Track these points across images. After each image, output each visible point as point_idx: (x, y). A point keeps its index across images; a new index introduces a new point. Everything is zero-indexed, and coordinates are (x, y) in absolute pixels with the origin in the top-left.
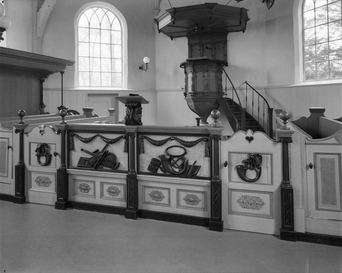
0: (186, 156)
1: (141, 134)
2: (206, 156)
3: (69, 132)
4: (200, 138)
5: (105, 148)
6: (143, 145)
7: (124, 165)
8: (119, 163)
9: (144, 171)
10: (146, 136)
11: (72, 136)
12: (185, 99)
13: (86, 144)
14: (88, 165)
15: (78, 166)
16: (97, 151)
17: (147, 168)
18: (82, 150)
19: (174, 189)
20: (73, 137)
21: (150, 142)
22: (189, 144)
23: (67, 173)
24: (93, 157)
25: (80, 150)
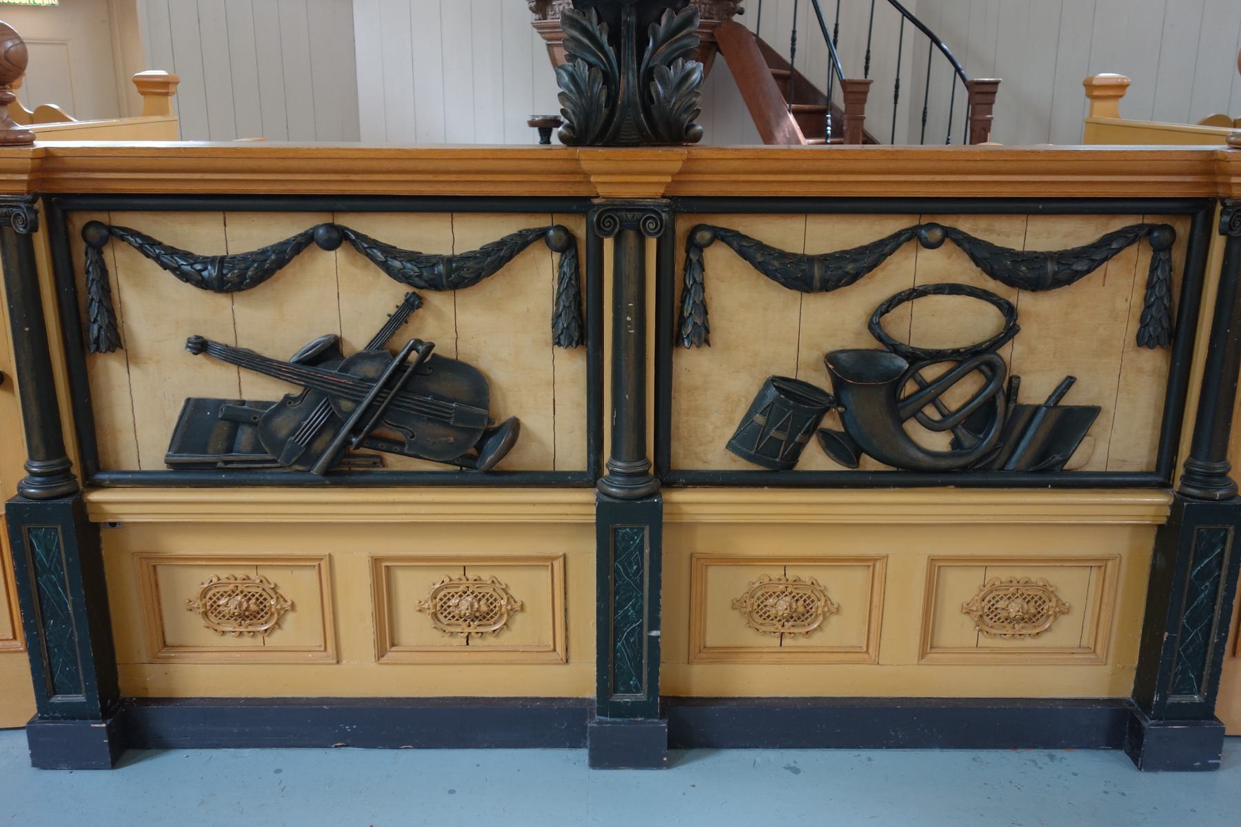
0: (1005, 352)
2: (1144, 340)
4: (1117, 224)
5: (399, 319)
7: (547, 436)
8: (515, 425)
9: (700, 466)
10: (723, 222)
11: (96, 248)
12: (538, 27)
13: (222, 300)
14: (257, 448)
15: (176, 466)
16: (330, 351)
18: (200, 346)
19: (918, 551)
20: (100, 253)
22: (1051, 267)
23: (92, 519)
24: (296, 391)
25: (177, 345)
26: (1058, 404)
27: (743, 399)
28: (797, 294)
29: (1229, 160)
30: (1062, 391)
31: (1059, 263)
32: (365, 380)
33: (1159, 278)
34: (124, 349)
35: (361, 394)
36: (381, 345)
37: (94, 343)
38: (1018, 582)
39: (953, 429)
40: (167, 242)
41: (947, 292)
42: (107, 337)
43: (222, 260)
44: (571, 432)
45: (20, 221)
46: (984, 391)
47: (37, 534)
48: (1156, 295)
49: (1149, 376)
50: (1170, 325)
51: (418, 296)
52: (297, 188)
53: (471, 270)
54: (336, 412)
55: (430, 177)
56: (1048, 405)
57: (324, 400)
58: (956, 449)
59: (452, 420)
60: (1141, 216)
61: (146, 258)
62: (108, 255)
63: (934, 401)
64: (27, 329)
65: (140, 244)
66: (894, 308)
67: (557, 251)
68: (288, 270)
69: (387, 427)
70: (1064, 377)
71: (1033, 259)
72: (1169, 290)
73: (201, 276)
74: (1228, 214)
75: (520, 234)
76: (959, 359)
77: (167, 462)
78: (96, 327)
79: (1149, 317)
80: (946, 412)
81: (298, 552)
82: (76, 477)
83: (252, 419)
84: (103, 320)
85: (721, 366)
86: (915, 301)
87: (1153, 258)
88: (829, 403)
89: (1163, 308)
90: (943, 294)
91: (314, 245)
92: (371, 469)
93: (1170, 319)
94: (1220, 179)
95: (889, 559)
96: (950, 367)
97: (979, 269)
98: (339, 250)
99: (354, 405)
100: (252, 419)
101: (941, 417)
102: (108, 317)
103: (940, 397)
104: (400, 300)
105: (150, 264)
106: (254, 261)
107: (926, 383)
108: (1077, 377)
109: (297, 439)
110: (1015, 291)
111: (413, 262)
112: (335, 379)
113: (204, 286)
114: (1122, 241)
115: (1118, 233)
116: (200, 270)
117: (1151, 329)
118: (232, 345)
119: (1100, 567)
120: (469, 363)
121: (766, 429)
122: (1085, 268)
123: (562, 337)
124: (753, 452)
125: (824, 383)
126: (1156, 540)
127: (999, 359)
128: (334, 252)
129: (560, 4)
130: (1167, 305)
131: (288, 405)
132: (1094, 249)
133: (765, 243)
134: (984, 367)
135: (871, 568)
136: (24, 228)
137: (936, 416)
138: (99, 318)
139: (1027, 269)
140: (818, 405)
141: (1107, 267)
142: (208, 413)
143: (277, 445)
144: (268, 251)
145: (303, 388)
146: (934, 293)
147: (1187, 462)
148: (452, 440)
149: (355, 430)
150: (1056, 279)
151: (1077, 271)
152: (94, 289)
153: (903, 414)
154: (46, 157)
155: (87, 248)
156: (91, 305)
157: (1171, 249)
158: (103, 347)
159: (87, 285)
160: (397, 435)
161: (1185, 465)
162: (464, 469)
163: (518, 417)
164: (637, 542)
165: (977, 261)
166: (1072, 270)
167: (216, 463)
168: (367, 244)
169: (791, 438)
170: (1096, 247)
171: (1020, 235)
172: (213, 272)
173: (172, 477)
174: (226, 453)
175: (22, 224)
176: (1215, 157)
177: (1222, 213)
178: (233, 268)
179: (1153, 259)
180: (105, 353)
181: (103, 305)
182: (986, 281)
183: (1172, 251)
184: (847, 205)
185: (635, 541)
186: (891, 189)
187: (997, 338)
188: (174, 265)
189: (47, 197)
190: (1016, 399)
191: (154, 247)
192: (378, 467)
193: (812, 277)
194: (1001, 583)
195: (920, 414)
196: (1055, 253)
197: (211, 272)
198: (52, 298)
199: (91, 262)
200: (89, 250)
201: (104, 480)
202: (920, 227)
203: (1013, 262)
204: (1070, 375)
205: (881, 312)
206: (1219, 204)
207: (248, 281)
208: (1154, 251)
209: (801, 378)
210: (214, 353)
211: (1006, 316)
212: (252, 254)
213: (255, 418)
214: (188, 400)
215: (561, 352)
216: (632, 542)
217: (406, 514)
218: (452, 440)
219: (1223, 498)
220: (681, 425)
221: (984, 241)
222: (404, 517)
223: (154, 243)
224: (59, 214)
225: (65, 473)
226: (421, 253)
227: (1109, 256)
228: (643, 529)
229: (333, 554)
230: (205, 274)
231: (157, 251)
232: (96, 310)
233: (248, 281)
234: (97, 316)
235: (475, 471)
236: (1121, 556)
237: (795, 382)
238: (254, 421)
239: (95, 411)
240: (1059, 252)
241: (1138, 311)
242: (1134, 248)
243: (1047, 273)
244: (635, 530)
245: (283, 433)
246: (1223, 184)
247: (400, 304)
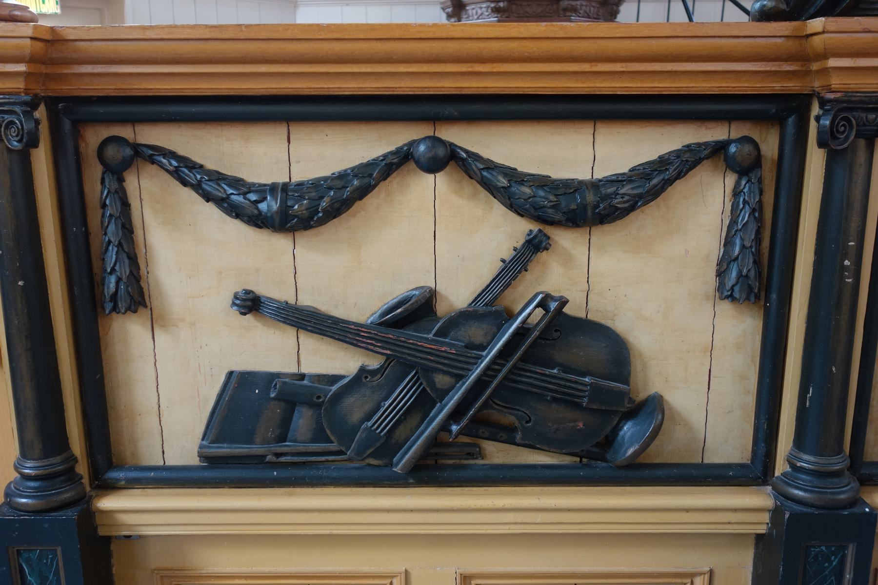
3: (78, 124)
7: (696, 418)
13: (280, 242)
14: (319, 435)
15: (211, 461)
20: (121, 180)
23: (102, 532)
24: (374, 362)
32: (471, 346)
34: (149, 308)
35: (466, 366)
36: (490, 300)
37: (111, 301)
40: (210, 165)
42: (129, 293)
43: (285, 187)
44: (729, 412)
45: (13, 131)
47: (29, 557)
51: (545, 235)
52: (397, 86)
53: (627, 198)
54: (428, 389)
55: (586, 67)
57: (413, 374)
59: (586, 400)
61: (181, 186)
62: (131, 182)
64: (21, 283)
65: (175, 167)
67: (734, 170)
68: (371, 201)
69: (495, 409)
73: (257, 208)
75: (688, 148)
77: (201, 456)
78: (113, 279)
81: (366, 569)
82: (82, 478)
83: (315, 399)
84: (124, 270)
91: (412, 165)
92: (466, 462)
98: (440, 176)
99: (453, 380)
100: (315, 399)
102: (130, 266)
104: (520, 242)
105: (188, 194)
106: (330, 188)
109: (376, 426)
111: (545, 188)
112: (433, 347)
113: (259, 223)
116: (255, 201)
118: (292, 301)
120: (603, 322)
123: (737, 289)
128: (432, 176)
129: (473, 9)
131: (364, 380)
136: (20, 141)
138: (117, 268)
142: (257, 391)
143: (347, 434)
144: (349, 174)
145: (385, 358)
148: (581, 425)
149: (456, 415)
152: (112, 228)
154: (54, 41)
155: (104, 173)
156: (107, 250)
158: (122, 305)
159: (102, 223)
160: (510, 419)
162: (584, 460)
163: (662, 393)
164: (834, 563)
167: (265, 456)
168: (483, 164)
172: (273, 203)
173: (207, 474)
174: (278, 442)
175: (17, 136)
178: (302, 197)
180: (124, 314)
181: (123, 250)
185: (830, 562)
188: (220, 194)
189: (52, 102)
191: (194, 171)
192: (476, 458)
197: (269, 206)
198: (55, 241)
199: (109, 192)
200: (106, 176)
201: (118, 480)
207: (321, 215)
210: (267, 312)
212: (325, 179)
213: (319, 397)
214: (231, 374)
215: (726, 307)
216: (827, 564)
217: (516, 523)
218: (581, 425)
222: (513, 527)
223: (193, 166)
224: (67, 125)
225: (69, 474)
226: (550, 177)
228: (845, 548)
229: (410, 571)
230: (263, 206)
231: (199, 177)
232: (114, 256)
233: (321, 215)
234: (115, 264)
235: (604, 464)
238: (317, 401)
239: (108, 388)
244: (833, 549)
245: (356, 416)
247: (519, 245)
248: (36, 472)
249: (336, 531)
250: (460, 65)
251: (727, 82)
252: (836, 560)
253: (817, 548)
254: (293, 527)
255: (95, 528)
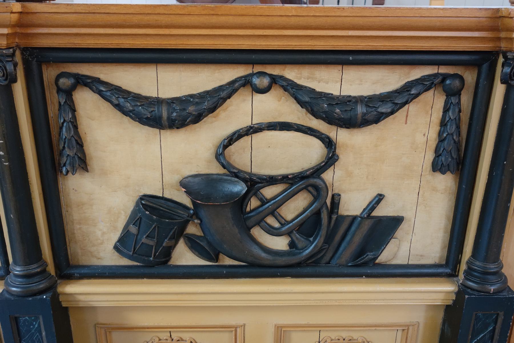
0: (327, 176)
1: (48, 62)
6: (76, 127)
17: (111, 246)
21: (118, 107)
22: (360, 109)
26: (371, 215)
27: (123, 212)
28: (157, 131)
29: (512, 16)
30: (373, 206)
31: (367, 106)
33: (450, 118)
38: (344, 340)
39: (289, 234)
41: (278, 128)
46: (311, 207)
48: (447, 132)
49: (442, 193)
50: (459, 155)
56: (362, 216)
58: (293, 248)
60: (436, 67)
63: (273, 213)
66: (235, 142)
70: (375, 194)
71: (346, 103)
72: (458, 127)
74: (509, 65)
76: (290, 182)
79: (442, 149)
80: (283, 221)
85: (101, 187)
86: (254, 136)
87: (446, 101)
88: (188, 216)
89: (452, 142)
90: (275, 130)
93: (459, 150)
94: (503, 35)
95: (246, 327)
96: (285, 187)
97: (304, 110)
101: (280, 225)
103: (278, 210)
107: (266, 199)
108: (385, 195)
110: (334, 128)
114: (420, 88)
115: (417, 80)
117: (443, 159)
119: (403, 330)
121: (139, 237)
122: (389, 110)
124: (131, 253)
125: (186, 200)
126: (445, 312)
127: (321, 183)
130: (456, 140)
132: (396, 94)
133: (124, 88)
134: (310, 188)
135: (234, 332)
137: (277, 225)
139: (340, 111)
140: (179, 218)
141: (408, 108)
146: (268, 130)
147: (469, 260)
150: (365, 119)
151: (382, 113)
153: (249, 223)
157: (460, 95)
161: (467, 262)
164: (36, 326)
165: (302, 104)
166: (379, 112)
169: (159, 243)
170: (398, 93)
171: (337, 82)
176: (500, 14)
177: (503, 65)
179: (446, 103)
182: (310, 120)
183: (461, 96)
184: (185, 56)
185: (34, 326)
186: (219, 43)
187: (318, 167)
189: (25, 50)
190: (338, 212)
193: (160, 117)
194: (332, 340)
195: (263, 224)
196: (366, 97)
202: (252, 75)
203: (329, 105)
204: (380, 193)
205: (224, 145)
206: (501, 56)
208: (446, 96)
209: (167, 195)
211: (327, 148)
219: (496, 292)
220: (76, 232)
221: (306, 87)
227: (410, 100)
228: (38, 318)
236: (419, 323)
237: (162, 198)
240: (368, 96)
241: (433, 143)
242: (430, 93)
243: (357, 114)
244: (33, 318)
246: (506, 38)
248: (21, 273)
249: (211, 304)
250: (154, 30)
251: (377, 43)
252: (37, 324)
253: (23, 318)
254: (248, 302)
255: (62, 305)
